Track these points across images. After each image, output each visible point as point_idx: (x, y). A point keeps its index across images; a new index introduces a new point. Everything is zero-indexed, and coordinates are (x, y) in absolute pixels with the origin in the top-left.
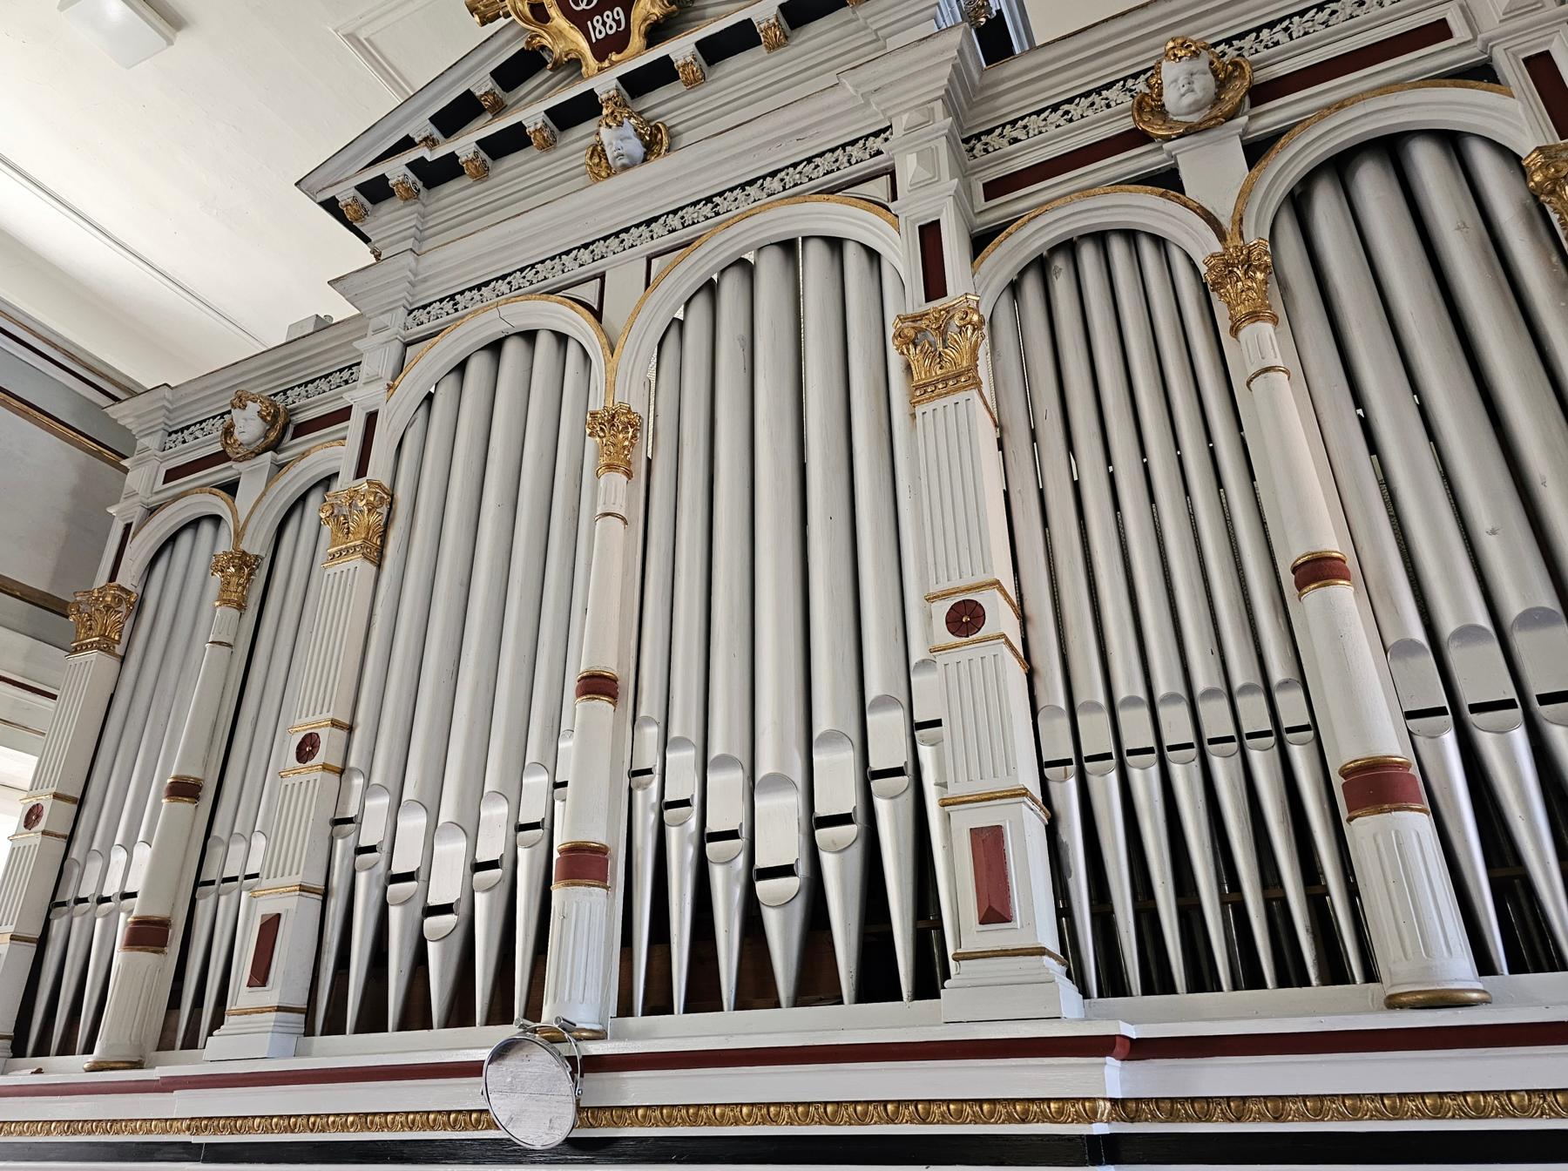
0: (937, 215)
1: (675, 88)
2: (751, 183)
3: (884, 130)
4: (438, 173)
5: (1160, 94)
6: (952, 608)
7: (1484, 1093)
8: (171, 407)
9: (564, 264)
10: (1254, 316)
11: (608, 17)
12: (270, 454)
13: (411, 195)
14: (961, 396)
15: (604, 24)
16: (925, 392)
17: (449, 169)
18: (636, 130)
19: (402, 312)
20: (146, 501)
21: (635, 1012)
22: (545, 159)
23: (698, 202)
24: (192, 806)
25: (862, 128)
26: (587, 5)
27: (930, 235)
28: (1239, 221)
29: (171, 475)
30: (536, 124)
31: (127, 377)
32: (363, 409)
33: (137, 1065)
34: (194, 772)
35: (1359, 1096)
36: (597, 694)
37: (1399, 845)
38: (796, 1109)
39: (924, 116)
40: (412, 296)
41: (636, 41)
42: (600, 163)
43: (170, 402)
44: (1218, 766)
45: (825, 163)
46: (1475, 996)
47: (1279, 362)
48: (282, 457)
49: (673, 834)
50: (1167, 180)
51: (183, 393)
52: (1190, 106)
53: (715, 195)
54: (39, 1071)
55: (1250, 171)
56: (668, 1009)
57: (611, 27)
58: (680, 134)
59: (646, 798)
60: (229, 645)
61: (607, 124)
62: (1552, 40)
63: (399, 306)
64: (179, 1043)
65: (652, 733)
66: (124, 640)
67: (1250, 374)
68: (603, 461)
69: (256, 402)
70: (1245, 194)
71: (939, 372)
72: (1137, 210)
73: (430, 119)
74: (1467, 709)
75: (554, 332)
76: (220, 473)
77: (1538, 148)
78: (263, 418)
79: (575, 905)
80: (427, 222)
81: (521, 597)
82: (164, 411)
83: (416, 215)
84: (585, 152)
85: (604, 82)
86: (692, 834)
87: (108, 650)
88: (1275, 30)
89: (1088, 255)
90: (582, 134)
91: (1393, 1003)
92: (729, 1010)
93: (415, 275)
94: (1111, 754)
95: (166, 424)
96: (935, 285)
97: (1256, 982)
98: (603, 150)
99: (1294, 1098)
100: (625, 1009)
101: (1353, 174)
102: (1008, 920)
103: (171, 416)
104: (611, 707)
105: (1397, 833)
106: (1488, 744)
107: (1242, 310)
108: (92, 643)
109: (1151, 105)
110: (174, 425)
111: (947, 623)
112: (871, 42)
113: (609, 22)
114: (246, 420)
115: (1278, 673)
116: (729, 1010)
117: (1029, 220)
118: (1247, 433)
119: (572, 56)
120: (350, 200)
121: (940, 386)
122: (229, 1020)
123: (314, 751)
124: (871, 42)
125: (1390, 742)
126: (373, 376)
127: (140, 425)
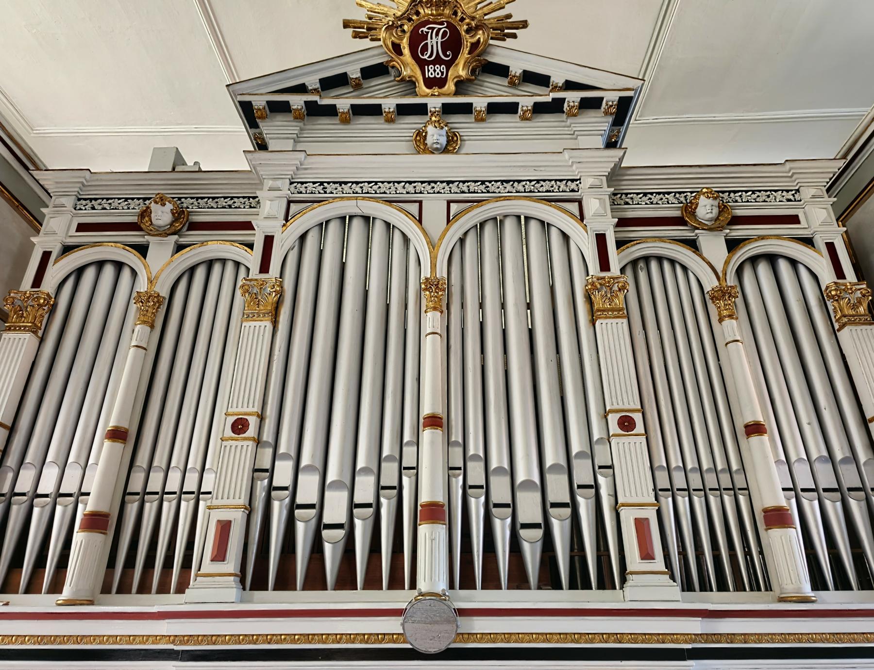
0: (604, 231)
1: (471, 118)
2: (507, 182)
3: (577, 180)
4: (314, 110)
5: (696, 208)
6: (620, 418)
7: (815, 634)
8: (86, 183)
9: (396, 188)
10: (731, 316)
11: (431, 68)
12: (176, 237)
13: (299, 117)
14: (619, 320)
15: (435, 71)
16: (603, 314)
17: (331, 111)
18: (447, 133)
19: (288, 182)
20: (65, 241)
21: (456, 587)
22: (386, 126)
23: (477, 181)
24: (122, 445)
25: (566, 176)
26: (428, 57)
27: (601, 239)
28: (725, 274)
29: (81, 227)
30: (389, 108)
31: (30, 148)
32: (264, 232)
33: (91, 603)
34: (125, 425)
35: (774, 634)
36: (436, 426)
37: (790, 541)
38: (560, 636)
39: (827, 288)
40: (295, 174)
41: (450, 86)
42: (420, 142)
43: (87, 181)
44: (712, 500)
45: (547, 186)
46: (813, 598)
47: (739, 339)
48: (183, 240)
49: (472, 501)
50: (692, 244)
51: (99, 178)
52: (709, 218)
53: (487, 181)
54: (7, 604)
55: (729, 253)
56: (149, 591)
57: (438, 74)
58: (465, 140)
59: (457, 482)
60: (145, 349)
61: (435, 125)
62: (835, 239)
63: (287, 178)
64: (114, 589)
65: (457, 452)
66: (43, 327)
67: (727, 342)
68: (431, 304)
69: (171, 203)
70: (727, 263)
71: (609, 306)
72: (686, 256)
73: (320, 80)
74: (800, 490)
75: (385, 222)
76: (134, 237)
77: (834, 282)
78: (173, 214)
79: (438, 533)
80: (303, 133)
81: (376, 364)
82: (80, 185)
83: (298, 128)
84: (414, 131)
85: (435, 103)
86: (265, 487)
87: (35, 333)
88: (736, 195)
89: (654, 265)
90: (413, 123)
91: (782, 600)
92: (505, 589)
93: (301, 165)
94: (461, 468)
95: (78, 193)
96: (605, 265)
97: (759, 589)
98: (426, 136)
99: (752, 634)
100: (452, 586)
101: (757, 266)
102: (654, 559)
103: (84, 189)
104: (441, 432)
105: (789, 536)
106: (805, 503)
107: (725, 313)
108: (25, 327)
109: (690, 209)
110: (82, 195)
111: (618, 424)
112: (570, 134)
113: (438, 71)
114: (162, 212)
115: (735, 466)
116: (505, 589)
117: (637, 244)
118: (721, 362)
119: (414, 79)
120: (261, 107)
121: (610, 313)
122: (629, 577)
123: (245, 429)
124: (570, 134)
125: (781, 500)
126: (272, 215)
127: (57, 188)
